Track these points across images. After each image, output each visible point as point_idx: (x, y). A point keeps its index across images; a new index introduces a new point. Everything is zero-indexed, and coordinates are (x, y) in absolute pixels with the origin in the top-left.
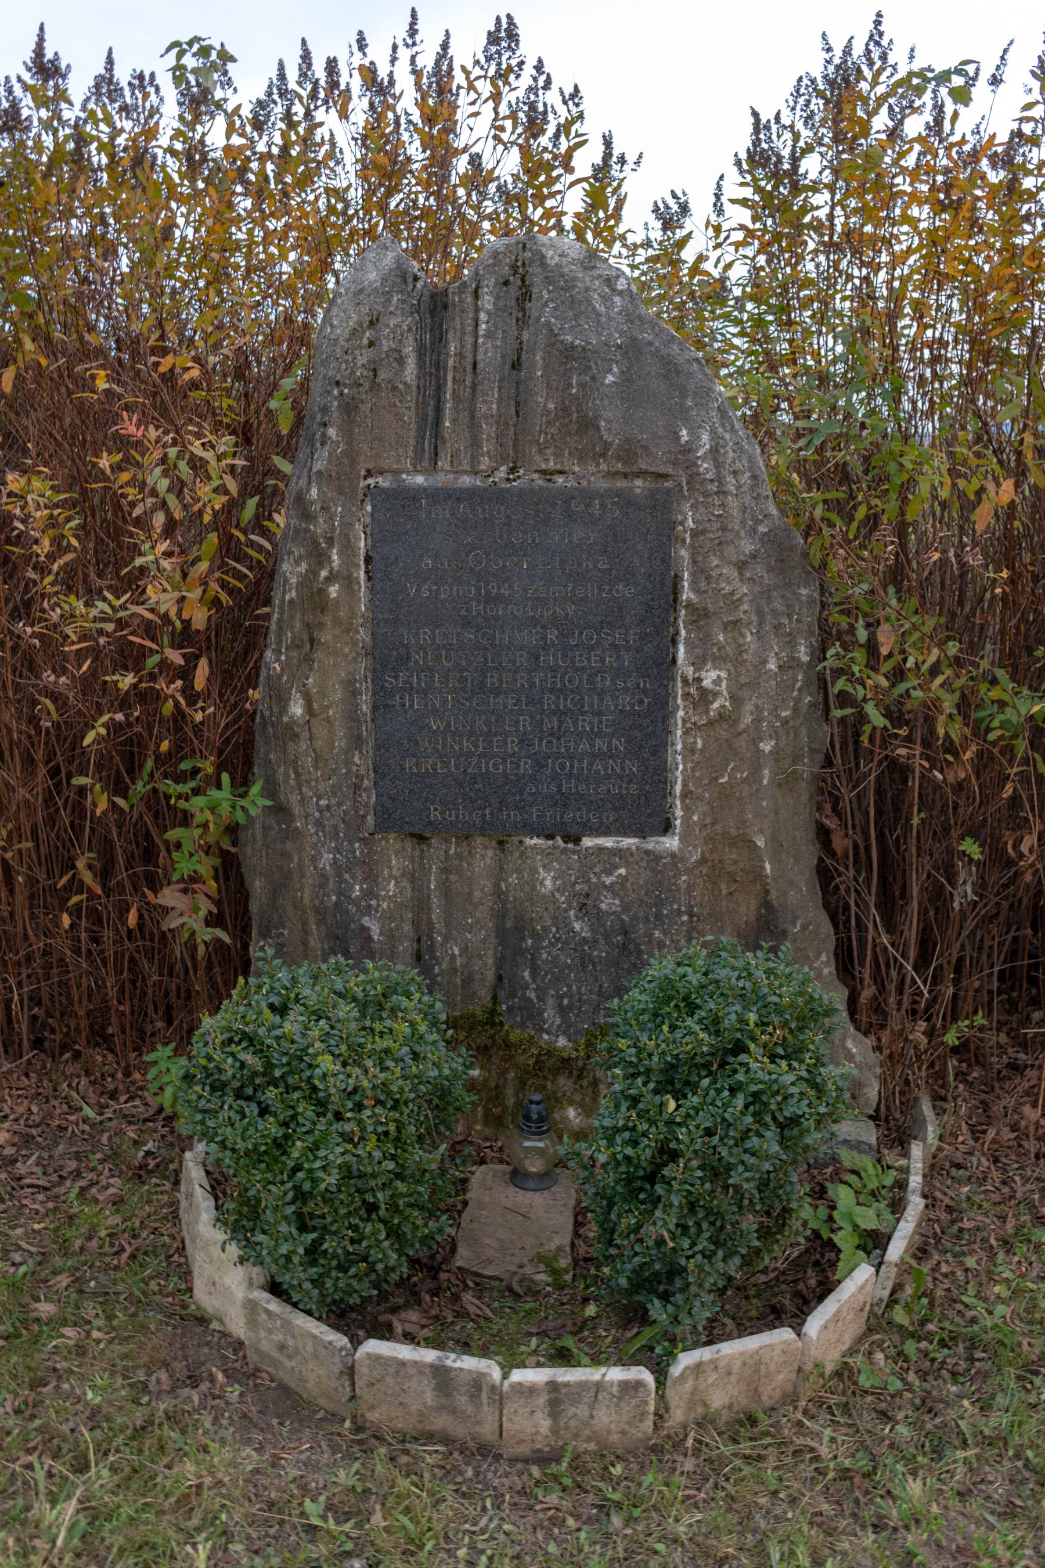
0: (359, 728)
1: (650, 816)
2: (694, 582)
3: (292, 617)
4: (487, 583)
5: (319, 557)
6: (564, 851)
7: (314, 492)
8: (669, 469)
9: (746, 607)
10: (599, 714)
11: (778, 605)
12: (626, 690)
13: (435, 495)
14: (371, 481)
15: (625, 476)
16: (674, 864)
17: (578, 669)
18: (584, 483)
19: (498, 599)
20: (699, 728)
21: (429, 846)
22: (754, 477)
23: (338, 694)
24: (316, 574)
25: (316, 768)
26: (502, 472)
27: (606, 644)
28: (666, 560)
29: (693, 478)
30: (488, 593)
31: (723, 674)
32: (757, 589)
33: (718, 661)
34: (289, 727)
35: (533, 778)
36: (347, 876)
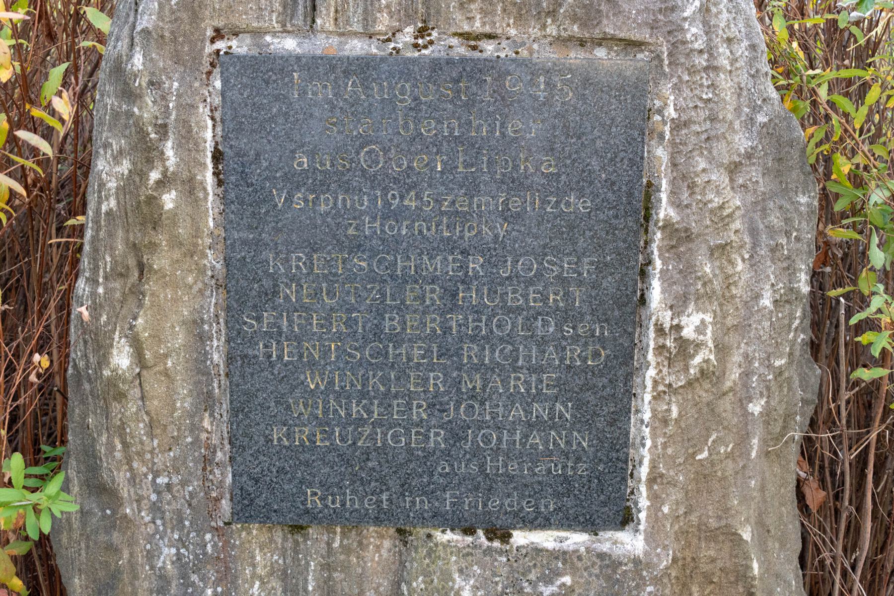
0: (209, 383)
1: (604, 504)
2: (674, 193)
3: (111, 235)
4: (385, 191)
5: (146, 152)
6: (489, 551)
7: (138, 61)
8: (643, 35)
9: (737, 225)
10: (538, 370)
11: (775, 220)
12: (576, 338)
13: (311, 65)
14: (221, 45)
15: (582, 43)
16: (638, 572)
17: (510, 310)
18: (524, 53)
19: (397, 215)
20: (676, 392)
21: (306, 537)
22: (753, 47)
23: (179, 339)
24: (143, 176)
25: (152, 437)
26: (407, 35)
27: (550, 276)
28: (637, 162)
29: (678, 45)
30: (387, 204)
31: (708, 318)
32: (750, 198)
33: (703, 299)
34: (112, 383)
35: (447, 453)
36: (194, 578)
